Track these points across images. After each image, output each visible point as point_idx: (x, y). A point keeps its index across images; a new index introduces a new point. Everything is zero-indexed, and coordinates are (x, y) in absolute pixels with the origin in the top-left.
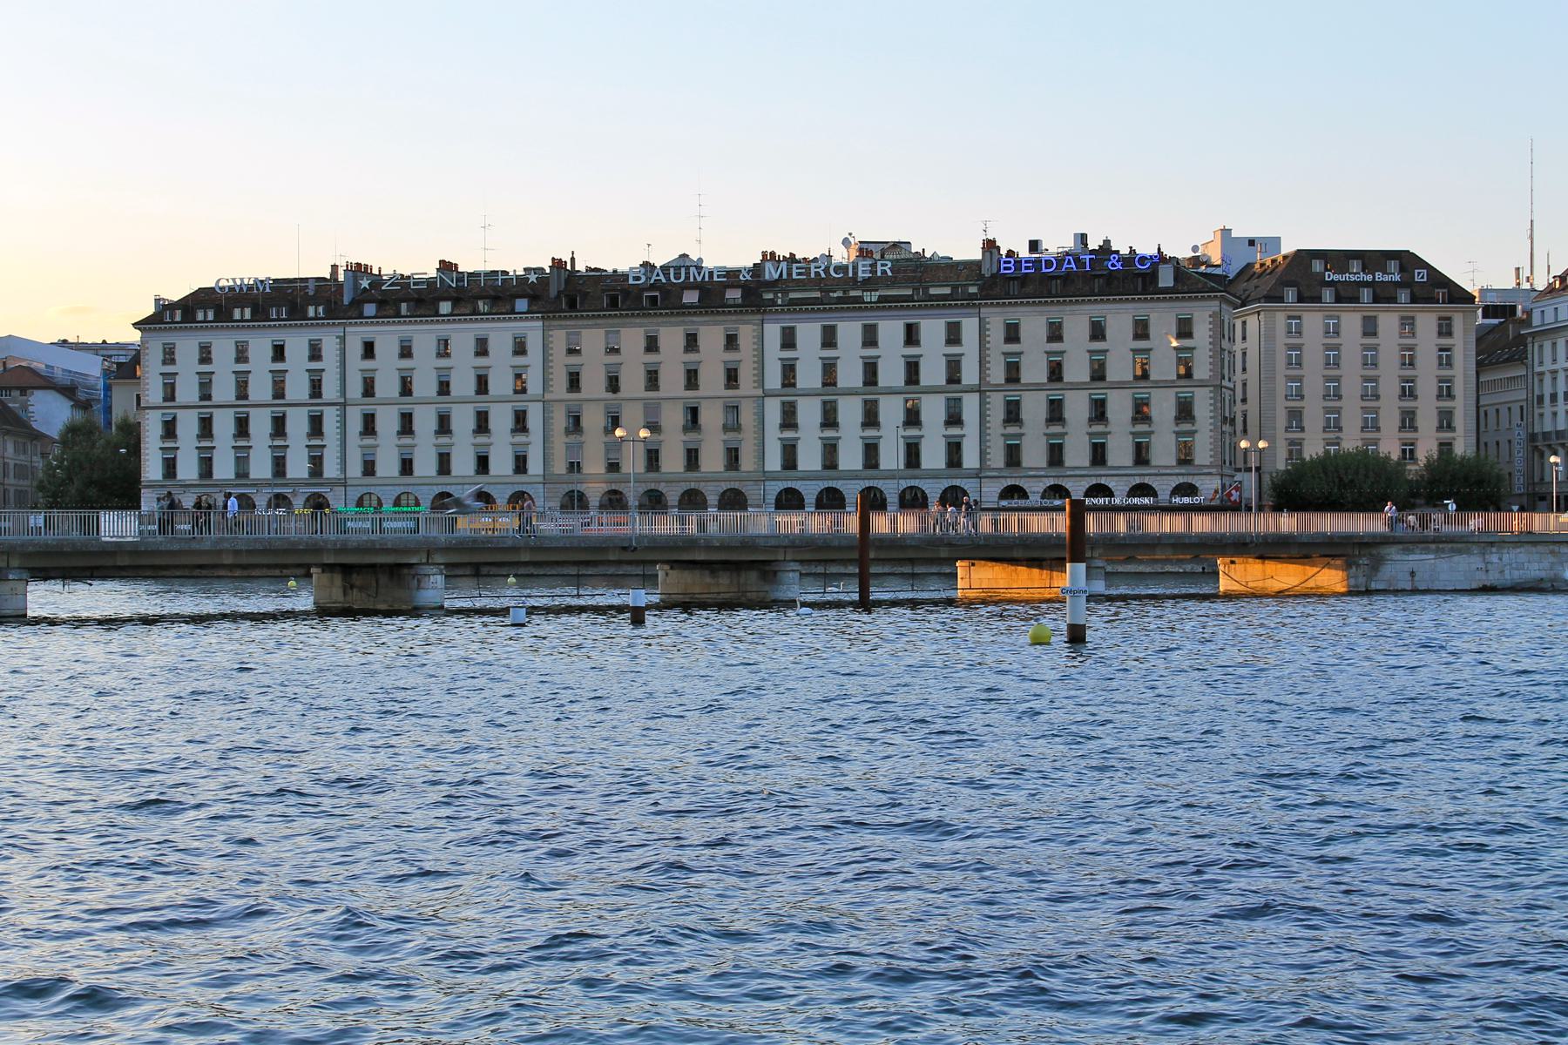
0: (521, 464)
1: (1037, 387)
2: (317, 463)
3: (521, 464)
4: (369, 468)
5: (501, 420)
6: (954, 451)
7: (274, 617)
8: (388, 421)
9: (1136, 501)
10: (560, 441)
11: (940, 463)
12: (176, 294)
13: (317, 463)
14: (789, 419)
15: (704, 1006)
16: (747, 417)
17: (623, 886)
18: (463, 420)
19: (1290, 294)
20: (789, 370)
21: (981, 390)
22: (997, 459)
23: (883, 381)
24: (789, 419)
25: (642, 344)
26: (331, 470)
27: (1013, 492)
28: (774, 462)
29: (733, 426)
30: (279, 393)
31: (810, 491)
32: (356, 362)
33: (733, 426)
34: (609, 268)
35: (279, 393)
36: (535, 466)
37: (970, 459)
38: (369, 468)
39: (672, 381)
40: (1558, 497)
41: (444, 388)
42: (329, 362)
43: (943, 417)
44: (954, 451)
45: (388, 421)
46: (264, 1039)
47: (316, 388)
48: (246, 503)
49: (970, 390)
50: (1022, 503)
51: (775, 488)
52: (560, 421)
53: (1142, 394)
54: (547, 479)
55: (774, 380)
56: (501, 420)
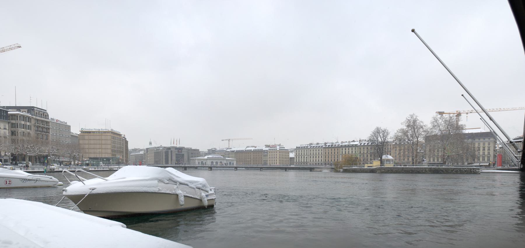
0: (321, 160)
1: (366, 154)
2: (307, 160)
3: (321, 160)
5: (320, 157)
8: (312, 157)
9: (469, 165)
10: (309, 158)
13: (307, 160)
15: (18, 193)
16: (339, 156)
17: (510, 210)
19: (398, 143)
20: (342, 152)
21: (309, 155)
26: (308, 161)
29: (338, 157)
30: (319, 154)
33: (338, 157)
34: (193, 148)
36: (323, 161)
39: (333, 153)
40: (429, 166)
42: (308, 152)
45: (312, 157)
48: (304, 164)
55: (341, 153)
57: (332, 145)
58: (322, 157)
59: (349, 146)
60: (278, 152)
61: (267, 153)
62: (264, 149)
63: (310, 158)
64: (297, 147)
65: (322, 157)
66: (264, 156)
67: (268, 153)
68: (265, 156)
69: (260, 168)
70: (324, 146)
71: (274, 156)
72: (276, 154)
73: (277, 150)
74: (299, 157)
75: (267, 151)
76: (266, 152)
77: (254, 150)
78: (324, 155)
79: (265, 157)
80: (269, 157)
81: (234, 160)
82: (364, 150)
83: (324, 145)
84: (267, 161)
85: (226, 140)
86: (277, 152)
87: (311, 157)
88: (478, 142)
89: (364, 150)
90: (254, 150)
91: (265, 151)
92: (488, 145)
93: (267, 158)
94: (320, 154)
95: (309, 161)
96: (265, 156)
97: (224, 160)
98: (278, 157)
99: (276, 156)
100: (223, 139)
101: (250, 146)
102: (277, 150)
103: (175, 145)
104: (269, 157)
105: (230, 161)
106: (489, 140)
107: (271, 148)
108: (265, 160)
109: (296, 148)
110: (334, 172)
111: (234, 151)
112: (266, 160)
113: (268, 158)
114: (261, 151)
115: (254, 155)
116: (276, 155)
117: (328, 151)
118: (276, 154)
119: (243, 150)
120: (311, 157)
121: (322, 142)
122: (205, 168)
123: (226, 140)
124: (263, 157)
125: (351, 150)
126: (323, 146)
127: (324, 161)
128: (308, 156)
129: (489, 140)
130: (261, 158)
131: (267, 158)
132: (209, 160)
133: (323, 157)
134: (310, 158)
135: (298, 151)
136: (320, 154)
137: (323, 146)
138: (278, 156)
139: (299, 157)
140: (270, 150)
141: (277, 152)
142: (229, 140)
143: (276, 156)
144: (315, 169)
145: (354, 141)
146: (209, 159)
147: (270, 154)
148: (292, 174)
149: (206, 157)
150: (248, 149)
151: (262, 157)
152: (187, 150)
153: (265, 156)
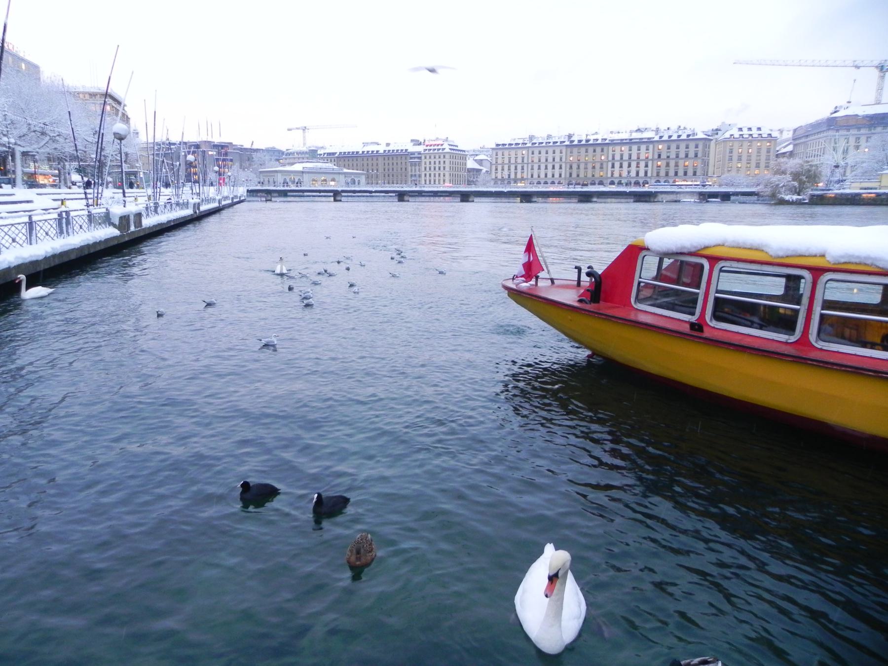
0: (560, 175)
3: (560, 175)
4: (532, 176)
5: (557, 166)
6: (646, 173)
7: (361, 196)
11: (643, 175)
12: (580, 134)
14: (613, 166)
18: (543, 167)
22: (655, 174)
23: (632, 158)
24: (613, 166)
25: (592, 151)
27: (658, 181)
28: (609, 175)
31: (616, 181)
32: (530, 155)
35: (630, 158)
36: (563, 176)
37: (649, 174)
38: (532, 176)
41: (547, 160)
43: (619, 166)
44: (646, 173)
46: (682, 302)
47: (561, 159)
49: (610, 161)
50: (659, 184)
51: (609, 181)
52: (568, 166)
53: (677, 161)
54: (565, 178)
56: (557, 166)
57: (587, 141)
58: (561, 168)
59: (630, 142)
60: (447, 156)
61: (420, 158)
62: (412, 148)
63: (532, 169)
64: (498, 145)
65: (561, 168)
66: (411, 165)
67: (423, 157)
68: (413, 164)
69: (332, 194)
70: (567, 143)
71: (437, 166)
72: (442, 160)
73: (445, 151)
74: (516, 169)
75: (419, 153)
76: (416, 155)
77: (385, 151)
78: (566, 163)
79: (413, 168)
80: (425, 168)
81: (362, 174)
82: (669, 152)
83: (566, 139)
84: (420, 176)
85: (297, 129)
86: (444, 157)
87: (532, 167)
88: (857, 136)
89: (669, 152)
90: (385, 151)
91: (413, 153)
92: (640, 153)
93: (419, 169)
94: (557, 159)
95: (530, 176)
96: (415, 165)
97: (339, 173)
98: (447, 169)
99: (442, 165)
100: (290, 127)
101: (370, 141)
102: (445, 151)
103: (210, 139)
104: (425, 168)
105: (353, 177)
106: (859, 133)
107: (429, 148)
108: (413, 173)
109: (494, 146)
110: (634, 202)
111: (334, 154)
112: (418, 173)
113: (423, 169)
114: (404, 155)
115: (387, 162)
116: (442, 163)
117: (621, 151)
118: (442, 160)
119: (357, 152)
120: (532, 167)
121: (559, 133)
122: (357, 194)
123: (297, 129)
124: (409, 168)
125: (515, 156)
126: (564, 142)
127: (568, 175)
128: (525, 166)
129: (859, 133)
130: (404, 170)
131: (419, 169)
132: (307, 175)
133: (566, 167)
134: (532, 169)
135: (500, 153)
136: (557, 159)
137: (564, 142)
138: (447, 165)
139: (516, 169)
140: (427, 152)
141: (444, 157)
142: (305, 129)
143: (442, 165)
144: (660, 197)
145: (638, 130)
146: (308, 173)
147: (428, 161)
148: (479, 208)
149: (298, 167)
150: (366, 149)
151: (406, 169)
152: (238, 149)
153: (413, 164)
